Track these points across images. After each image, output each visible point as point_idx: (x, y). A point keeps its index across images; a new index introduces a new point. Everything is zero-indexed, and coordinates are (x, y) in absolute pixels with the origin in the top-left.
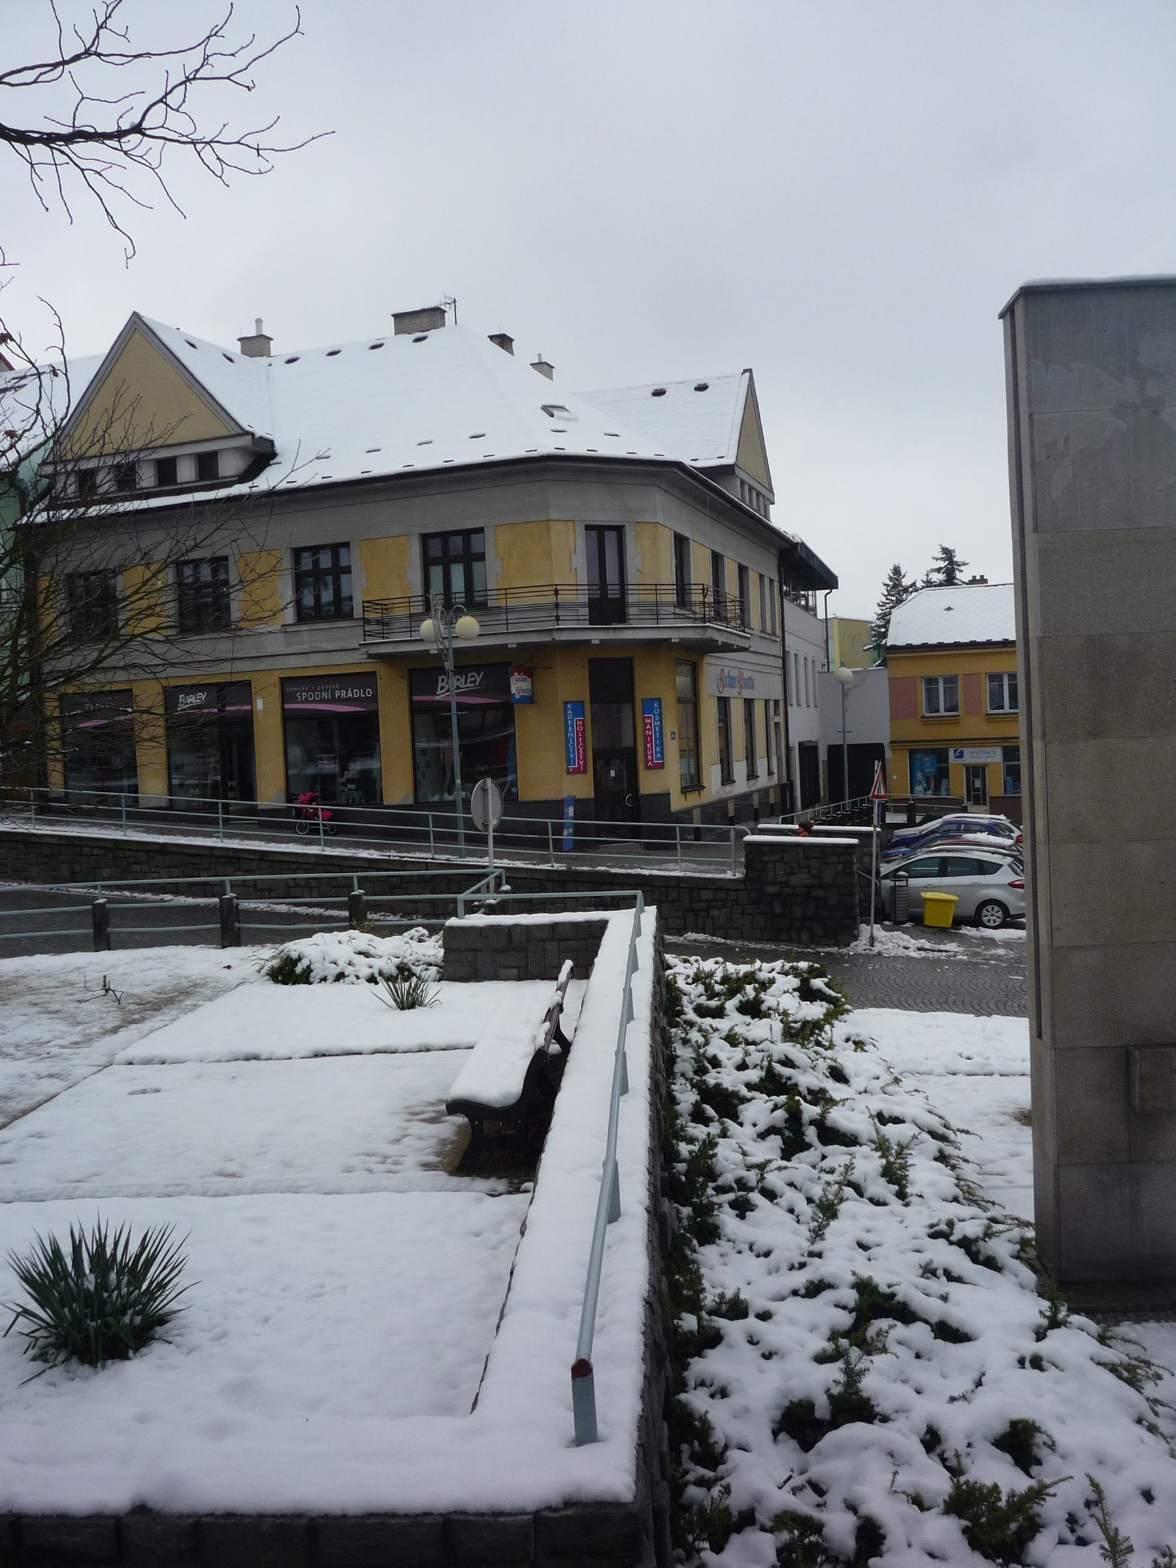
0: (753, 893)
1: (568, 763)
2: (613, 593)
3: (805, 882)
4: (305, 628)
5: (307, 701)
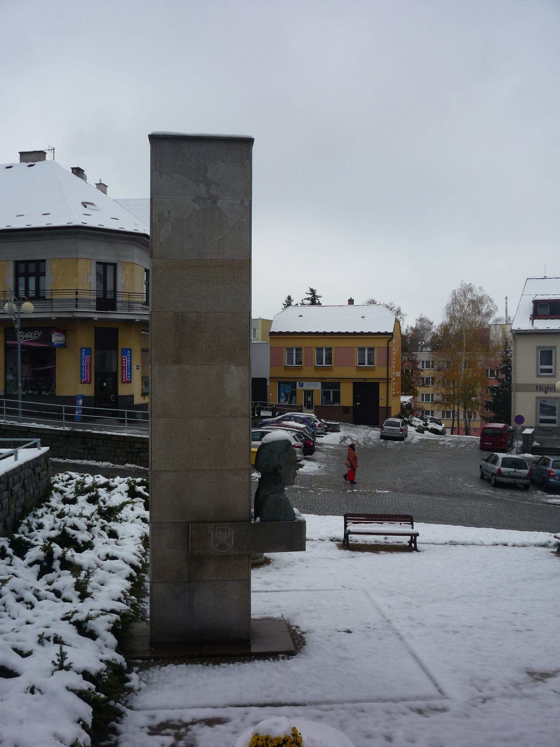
1: (82, 378)
2: (109, 296)
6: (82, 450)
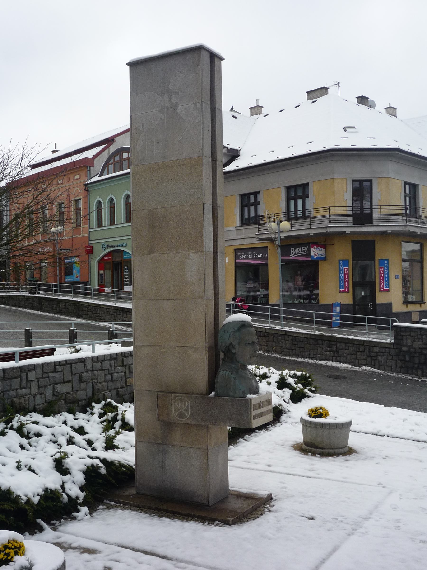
0: (397, 350)
1: (340, 288)
3: (421, 346)
4: (243, 228)
5: (244, 259)
6: (328, 353)
